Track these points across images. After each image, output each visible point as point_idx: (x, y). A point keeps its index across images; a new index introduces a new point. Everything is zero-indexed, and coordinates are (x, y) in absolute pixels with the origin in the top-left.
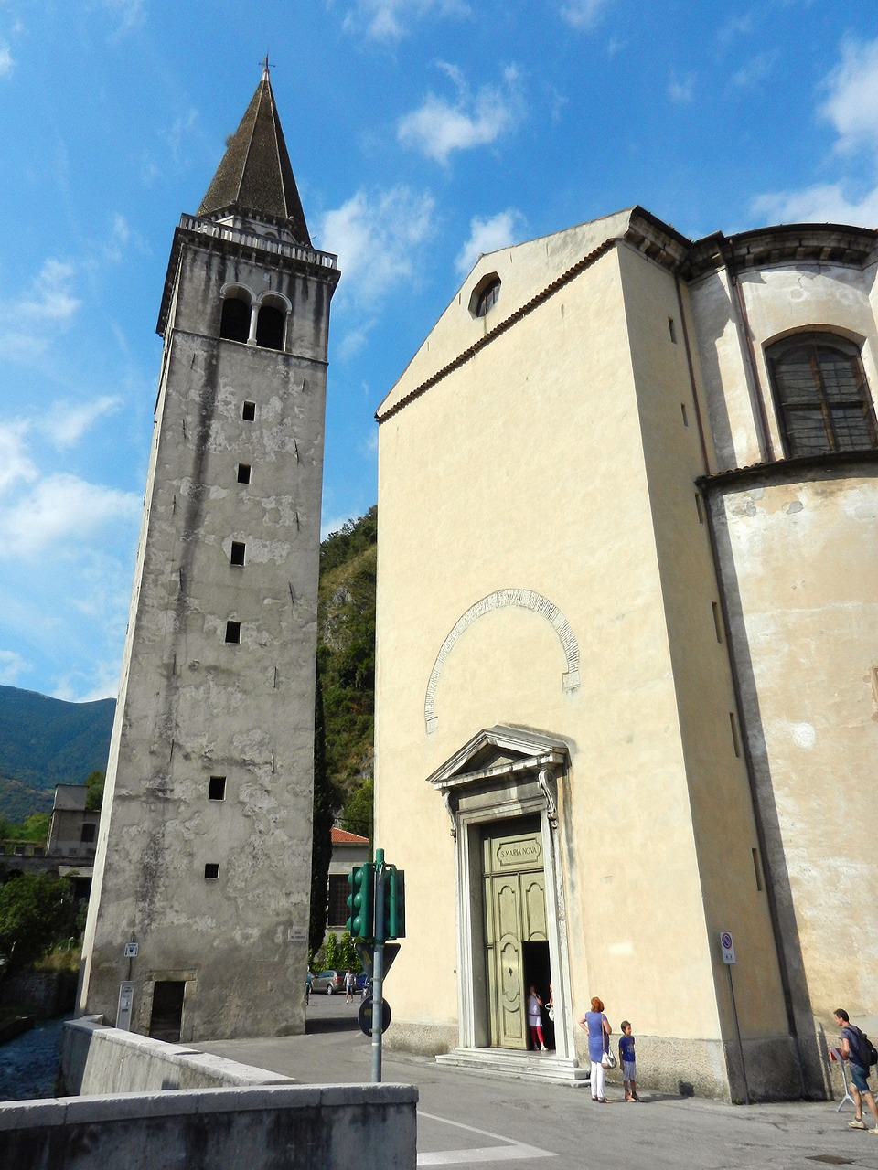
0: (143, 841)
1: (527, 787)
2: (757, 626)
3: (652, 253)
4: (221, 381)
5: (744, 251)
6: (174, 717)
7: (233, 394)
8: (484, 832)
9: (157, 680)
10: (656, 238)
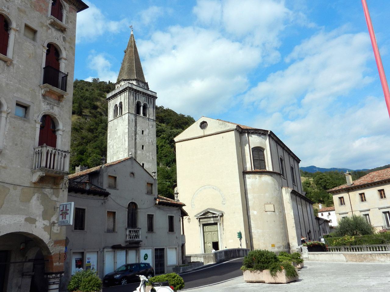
2: (250, 196)
7: (140, 128)
8: (204, 225)
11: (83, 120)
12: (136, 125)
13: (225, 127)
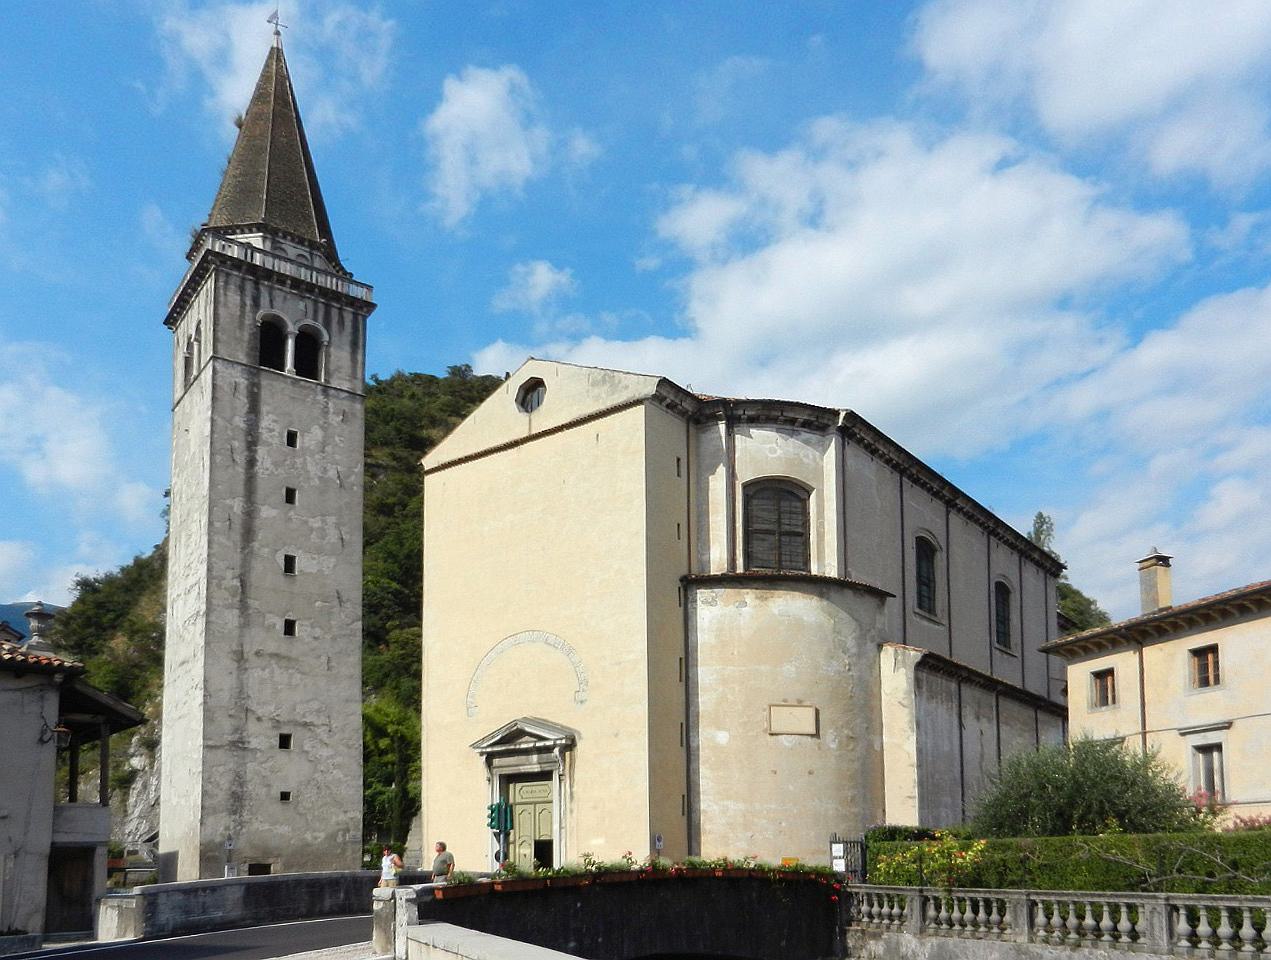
0: (230, 777)
1: (545, 755)
2: (706, 674)
3: (671, 406)
4: (264, 409)
5: (741, 412)
6: (246, 689)
7: (275, 421)
8: (507, 780)
9: (228, 663)
10: (676, 397)
12: (254, 408)
13: (613, 394)
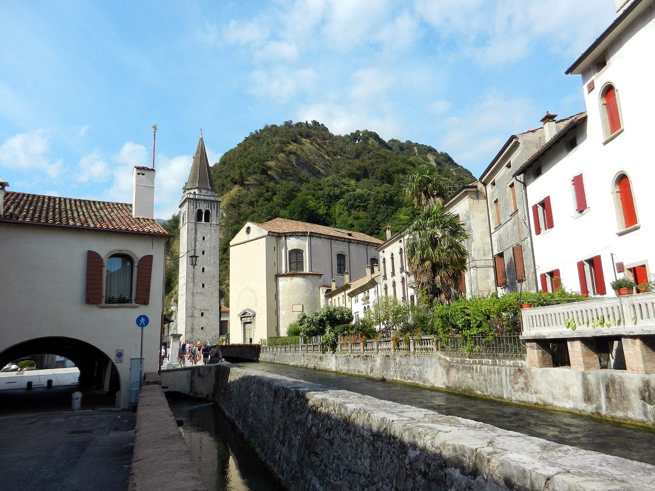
2: (281, 298)
4: (198, 232)
8: (245, 323)
11: (244, 191)
12: (196, 233)
